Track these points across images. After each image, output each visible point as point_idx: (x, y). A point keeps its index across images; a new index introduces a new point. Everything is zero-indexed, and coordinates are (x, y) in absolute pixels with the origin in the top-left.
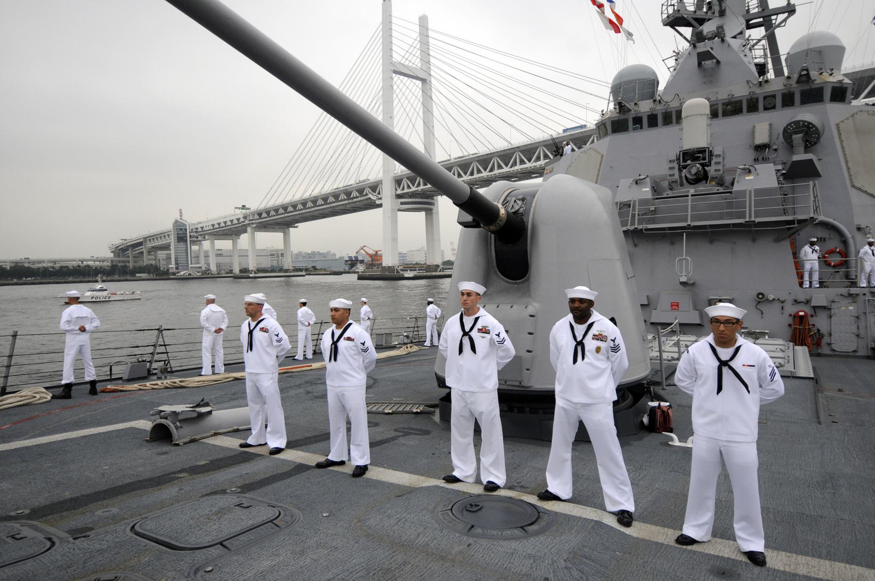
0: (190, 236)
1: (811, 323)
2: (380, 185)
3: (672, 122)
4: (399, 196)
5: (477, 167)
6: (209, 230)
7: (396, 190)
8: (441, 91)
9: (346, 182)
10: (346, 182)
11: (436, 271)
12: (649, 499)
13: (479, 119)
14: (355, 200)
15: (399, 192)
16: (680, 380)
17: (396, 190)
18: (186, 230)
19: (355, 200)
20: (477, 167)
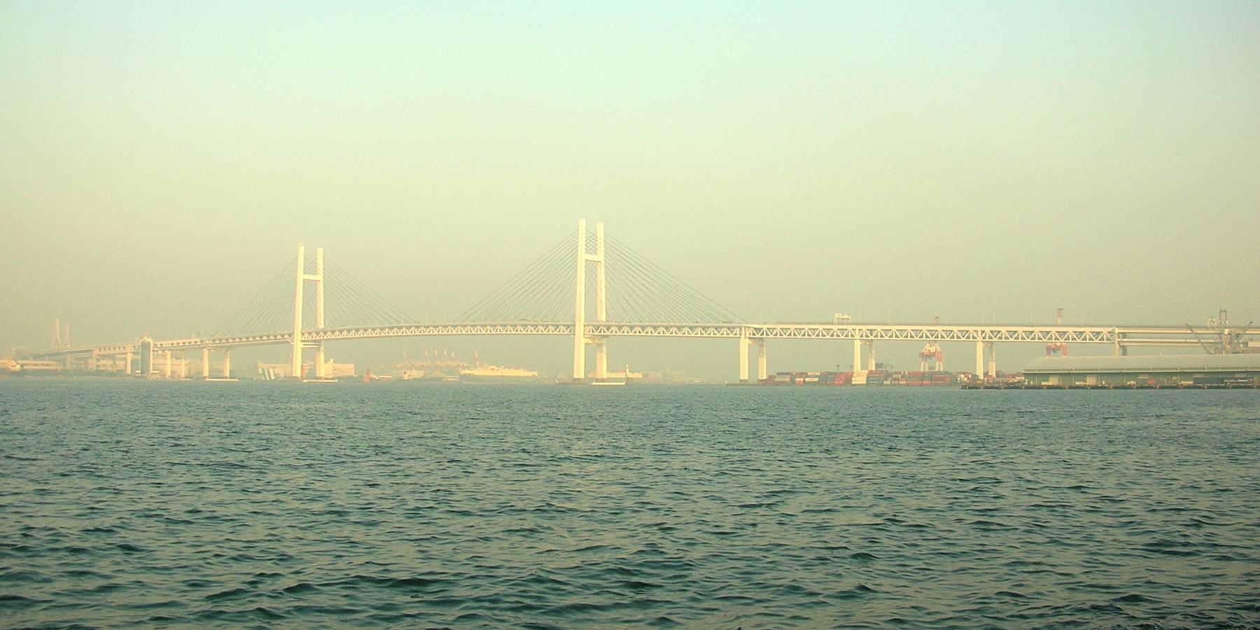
15: (303, 339)
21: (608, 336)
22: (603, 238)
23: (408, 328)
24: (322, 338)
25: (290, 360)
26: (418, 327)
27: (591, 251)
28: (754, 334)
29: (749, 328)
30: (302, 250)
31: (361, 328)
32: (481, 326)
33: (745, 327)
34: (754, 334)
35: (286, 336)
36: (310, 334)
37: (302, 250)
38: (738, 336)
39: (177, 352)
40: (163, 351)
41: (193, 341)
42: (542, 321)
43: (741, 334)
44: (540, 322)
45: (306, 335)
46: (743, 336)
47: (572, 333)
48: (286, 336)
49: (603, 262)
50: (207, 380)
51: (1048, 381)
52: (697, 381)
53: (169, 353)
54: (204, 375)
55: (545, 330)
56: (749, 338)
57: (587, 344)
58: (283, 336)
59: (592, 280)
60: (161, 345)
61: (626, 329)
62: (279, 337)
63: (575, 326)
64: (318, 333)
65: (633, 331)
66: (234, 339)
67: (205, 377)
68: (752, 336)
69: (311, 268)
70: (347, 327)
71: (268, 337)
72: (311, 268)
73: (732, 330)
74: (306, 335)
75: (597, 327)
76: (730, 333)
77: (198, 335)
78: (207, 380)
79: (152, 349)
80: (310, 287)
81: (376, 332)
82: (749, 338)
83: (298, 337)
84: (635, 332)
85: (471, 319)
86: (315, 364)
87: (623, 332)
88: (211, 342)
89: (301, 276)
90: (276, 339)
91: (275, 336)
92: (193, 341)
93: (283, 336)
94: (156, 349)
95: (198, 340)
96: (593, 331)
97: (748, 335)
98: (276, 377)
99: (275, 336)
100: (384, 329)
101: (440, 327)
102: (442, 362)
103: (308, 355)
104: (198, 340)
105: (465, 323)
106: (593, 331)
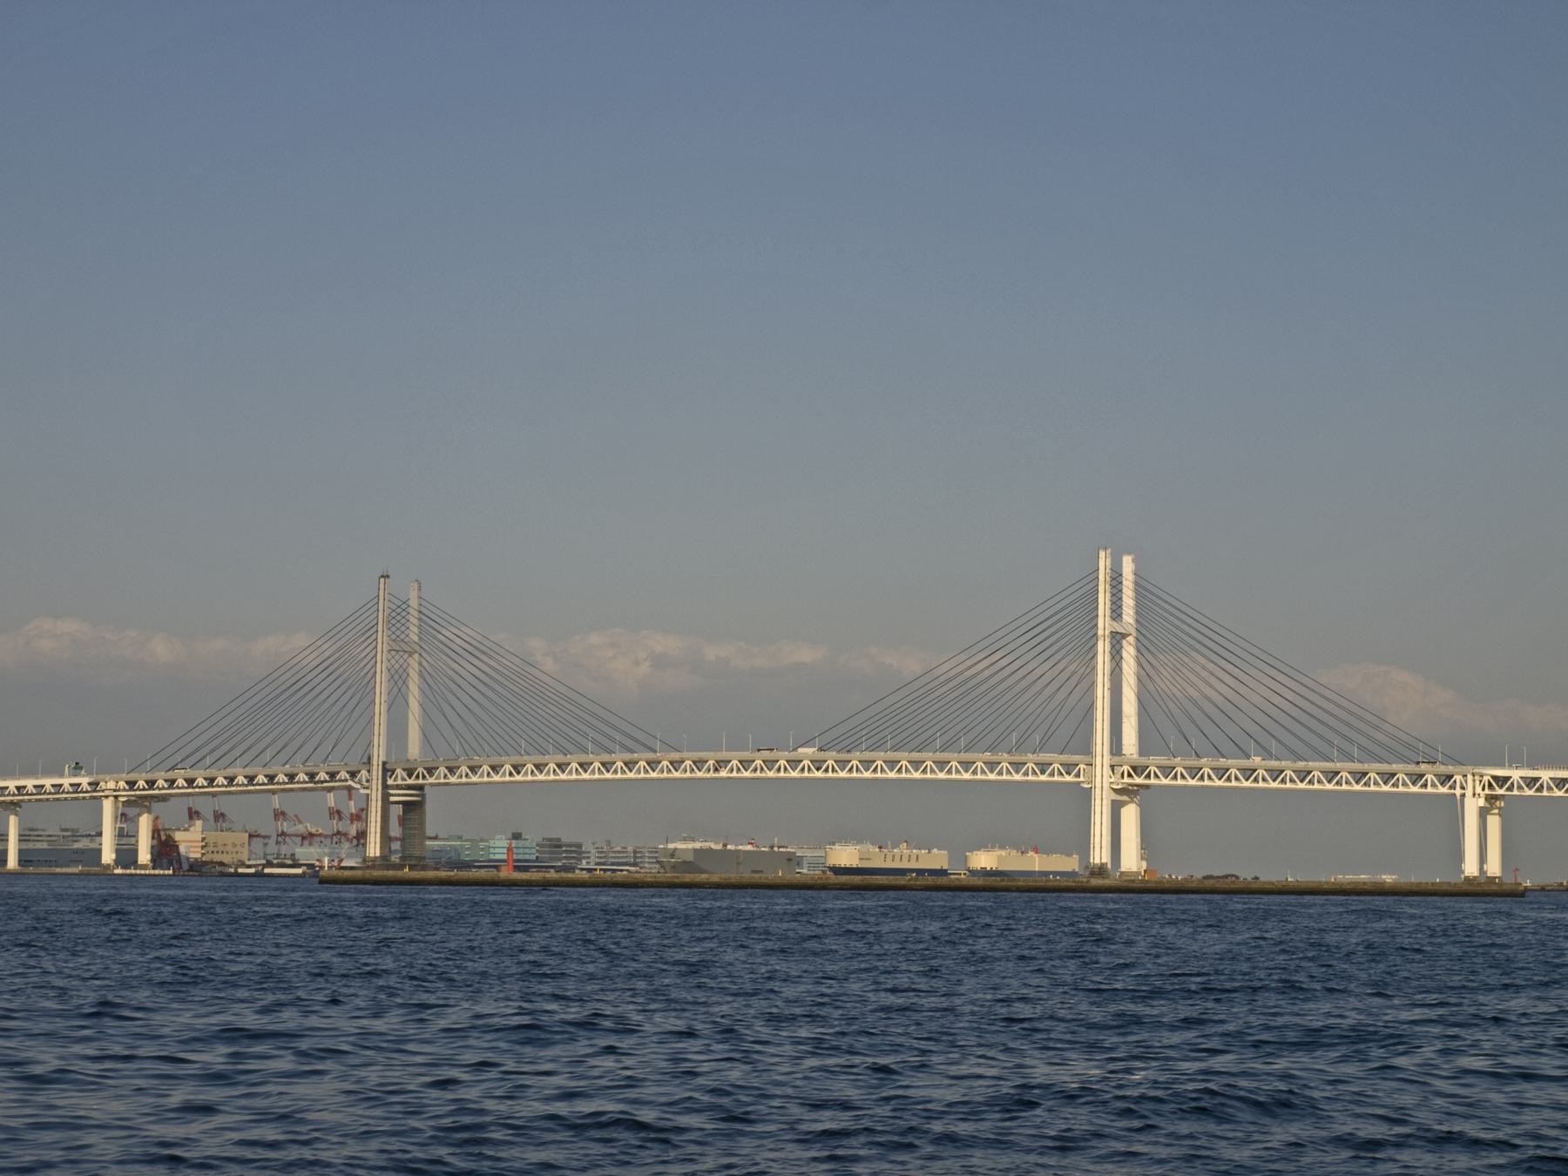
14: (325, 785)
41: (66, 782)
59: (400, 683)
77: (78, 768)
95: (84, 781)
104: (84, 781)
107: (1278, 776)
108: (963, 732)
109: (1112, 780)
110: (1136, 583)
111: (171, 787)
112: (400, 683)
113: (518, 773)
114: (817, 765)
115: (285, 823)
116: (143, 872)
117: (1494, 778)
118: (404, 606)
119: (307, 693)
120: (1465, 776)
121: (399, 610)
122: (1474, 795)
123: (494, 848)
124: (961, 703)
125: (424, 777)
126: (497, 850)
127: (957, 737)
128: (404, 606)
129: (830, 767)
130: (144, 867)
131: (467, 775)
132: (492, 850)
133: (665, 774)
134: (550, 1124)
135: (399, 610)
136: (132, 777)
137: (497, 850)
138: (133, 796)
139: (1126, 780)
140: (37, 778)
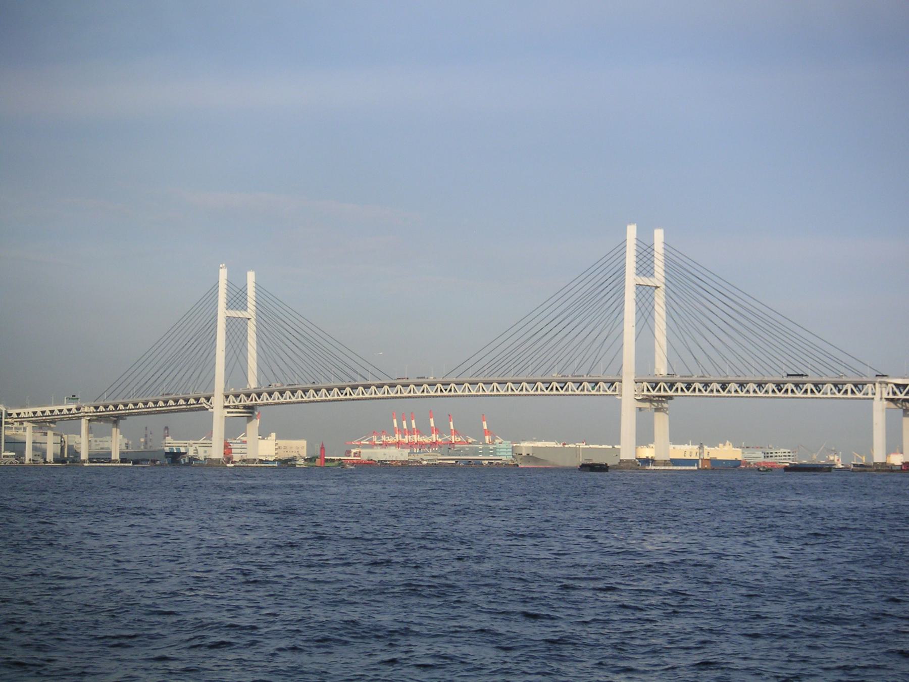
0: (5, 422)
1: (29, 462)
2: (212, 397)
3: (51, 403)
4: (226, 407)
5: (664, 387)
6: (29, 417)
7: (224, 402)
8: (289, 359)
9: (185, 390)
10: (185, 390)
11: (253, 463)
12: (319, 614)
13: (537, 368)
14: (192, 406)
15: (227, 404)
16: (881, 537)
17: (224, 402)
18: (727, 387)
19: (192, 406)
20: (664, 387)
21: (671, 398)
22: (662, 251)
23: (379, 386)
24: (254, 402)
25: (616, 438)
26: (392, 386)
27: (644, 272)
28: (894, 393)
29: (887, 384)
30: (223, 274)
31: (299, 389)
32: (499, 383)
33: (881, 383)
34: (894, 393)
35: (202, 400)
36: (237, 396)
37: (223, 274)
38: (870, 396)
39: (42, 424)
40: (21, 423)
41: (64, 408)
42: (182, 394)
43: (874, 394)
44: (570, 378)
45: (231, 397)
46: (877, 397)
47: (617, 393)
48: (202, 400)
49: (663, 286)
50: (85, 465)
51: (120, 434)
52: (805, 461)
53: (29, 426)
54: (82, 458)
55: (547, 389)
56: (887, 399)
57: (640, 409)
58: (197, 400)
59: (646, 314)
60: (18, 414)
61: (752, 387)
62: (192, 401)
63: (621, 382)
64: (248, 395)
65: (745, 390)
66: (125, 405)
67: (84, 461)
68: (891, 396)
69: (237, 299)
70: (173, 396)
71: (176, 401)
72: (237, 299)
73: (860, 386)
74: (231, 397)
75: (655, 385)
76: (836, 392)
77: (74, 398)
78: (85, 465)
79: (3, 420)
80: (236, 328)
81: (320, 393)
82: (887, 399)
83: (218, 401)
84: (712, 391)
85: (471, 372)
86: (88, 438)
87: (767, 392)
88: (92, 409)
89: (222, 313)
90: (187, 405)
91: (187, 400)
92: (64, 408)
93: (197, 400)
94: (10, 420)
95: (73, 407)
96: (648, 390)
97: (885, 396)
98: (190, 461)
99: (187, 400)
100: (408, 386)
101: (467, 385)
102: (440, 437)
103: (233, 430)
104: (73, 407)
105: (505, 378)
106: (648, 390)
107: (656, 386)
108: (555, 363)
109: (636, 393)
110: (665, 256)
111: (116, 410)
112: (646, 314)
113: (780, 391)
114: (562, 385)
115: (410, 437)
116: (114, 465)
117: (897, 385)
118: (649, 250)
119: (304, 344)
120: (874, 384)
121: (645, 253)
122: (881, 399)
123: (500, 449)
124: (775, 333)
125: (256, 400)
126: (501, 450)
127: (553, 366)
128: (649, 250)
129: (495, 388)
130: (115, 461)
131: (792, 391)
132: (498, 450)
133: (645, 393)
134: (172, 595)
135: (645, 253)
136: (96, 404)
137: (501, 450)
138: (95, 416)
139: (645, 393)
140: (51, 406)
